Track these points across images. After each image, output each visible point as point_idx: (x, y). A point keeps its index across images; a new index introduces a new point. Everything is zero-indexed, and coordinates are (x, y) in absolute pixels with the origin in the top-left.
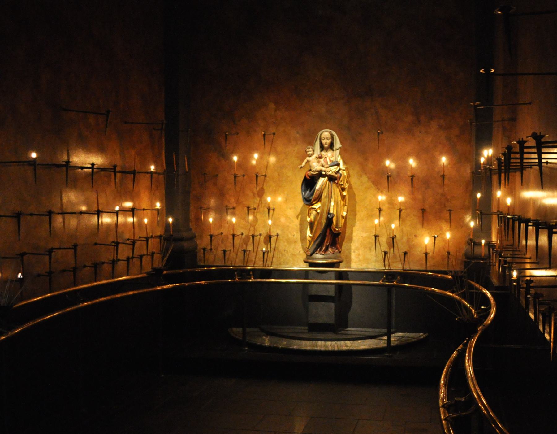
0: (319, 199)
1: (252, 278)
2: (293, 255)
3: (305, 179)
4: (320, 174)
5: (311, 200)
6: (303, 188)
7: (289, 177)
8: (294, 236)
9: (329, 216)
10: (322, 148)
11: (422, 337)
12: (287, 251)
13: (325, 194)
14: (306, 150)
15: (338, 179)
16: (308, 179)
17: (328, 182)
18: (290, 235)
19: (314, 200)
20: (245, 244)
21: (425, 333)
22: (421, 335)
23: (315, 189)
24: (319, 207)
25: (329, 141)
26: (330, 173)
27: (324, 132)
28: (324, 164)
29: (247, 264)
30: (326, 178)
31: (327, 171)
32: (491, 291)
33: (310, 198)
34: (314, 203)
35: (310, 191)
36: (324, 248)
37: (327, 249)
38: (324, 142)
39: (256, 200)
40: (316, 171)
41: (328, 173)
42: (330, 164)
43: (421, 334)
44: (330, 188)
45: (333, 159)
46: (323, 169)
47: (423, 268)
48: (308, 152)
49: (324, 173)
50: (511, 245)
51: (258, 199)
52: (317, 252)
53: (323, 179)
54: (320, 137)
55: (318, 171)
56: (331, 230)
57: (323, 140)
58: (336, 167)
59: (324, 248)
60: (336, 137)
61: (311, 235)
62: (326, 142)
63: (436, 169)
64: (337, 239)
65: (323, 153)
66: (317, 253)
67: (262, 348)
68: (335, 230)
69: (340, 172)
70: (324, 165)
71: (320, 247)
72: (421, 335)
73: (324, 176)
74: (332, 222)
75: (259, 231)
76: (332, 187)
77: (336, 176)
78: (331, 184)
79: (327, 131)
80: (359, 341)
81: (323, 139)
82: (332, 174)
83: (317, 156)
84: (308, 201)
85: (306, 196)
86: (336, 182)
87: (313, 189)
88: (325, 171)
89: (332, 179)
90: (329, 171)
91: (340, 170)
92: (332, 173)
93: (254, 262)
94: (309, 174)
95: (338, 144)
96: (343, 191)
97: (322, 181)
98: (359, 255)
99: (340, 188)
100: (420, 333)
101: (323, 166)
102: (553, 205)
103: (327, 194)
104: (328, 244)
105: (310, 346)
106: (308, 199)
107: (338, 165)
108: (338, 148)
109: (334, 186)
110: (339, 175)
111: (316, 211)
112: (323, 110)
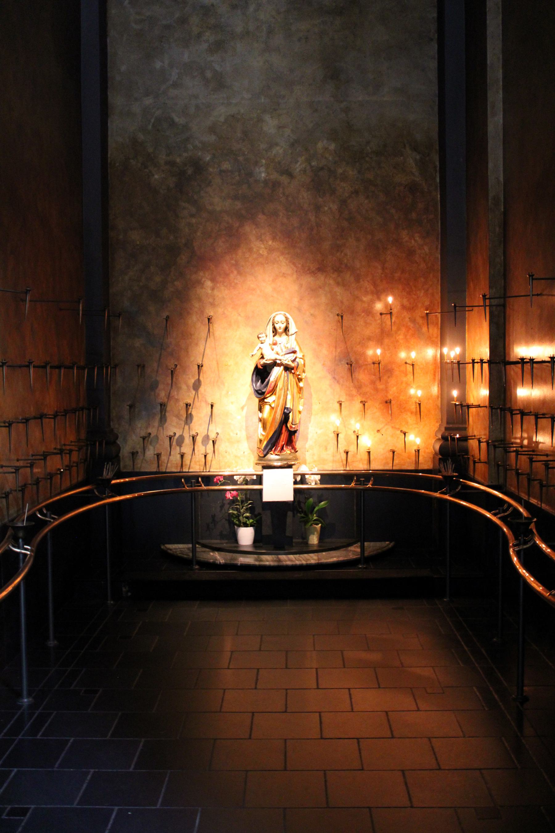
0: (273, 391)
1: (203, 486)
2: (236, 456)
3: (256, 368)
4: (275, 364)
5: (264, 392)
6: (254, 379)
7: (230, 366)
8: (237, 434)
9: (286, 410)
10: (275, 331)
11: (390, 546)
12: (229, 453)
13: (280, 385)
14: (258, 336)
15: (295, 369)
16: (260, 368)
17: (284, 371)
18: (232, 434)
19: (268, 393)
20: (178, 445)
21: (391, 542)
22: (386, 545)
23: (269, 380)
24: (274, 401)
25: (283, 326)
26: (286, 362)
27: (277, 315)
28: (280, 352)
29: (210, 469)
30: (282, 367)
31: (283, 360)
32: (452, 493)
33: (263, 391)
34: (268, 396)
35: (262, 382)
36: (279, 448)
37: (282, 449)
38: (277, 326)
39: (190, 394)
40: (269, 360)
41: (284, 361)
42: (286, 351)
43: (387, 543)
44: (286, 378)
45: (289, 346)
46: (278, 357)
47: (412, 467)
48: (261, 337)
49: (278, 362)
50: (501, 441)
51: (194, 392)
52: (272, 453)
53: (278, 368)
54: (273, 320)
55: (272, 360)
56: (287, 427)
57: (277, 323)
58: (293, 354)
59: (279, 448)
60: (291, 321)
61: (264, 433)
62: (280, 326)
63: (369, 360)
64: (293, 437)
65: (277, 338)
66: (271, 454)
67: (214, 566)
68: (291, 427)
69: (297, 360)
70: (279, 353)
71: (275, 447)
72: (386, 545)
73: (279, 365)
74: (288, 418)
75: (195, 430)
76: (288, 378)
77: (293, 365)
78: (287, 373)
79: (280, 314)
80: (324, 553)
81: (277, 322)
82: (288, 363)
83: (271, 343)
84: (261, 395)
85: (258, 389)
86: (293, 371)
87: (267, 380)
88: (280, 360)
89: (287, 369)
90: (285, 359)
91: (296, 358)
92: (289, 362)
93: (188, 466)
94: (262, 363)
95: (293, 328)
96: (299, 382)
97: (276, 372)
98: (314, 455)
99: (296, 378)
100: (386, 541)
101: (277, 354)
102: (527, 398)
103: (282, 386)
104: (284, 443)
105: (272, 561)
106: (260, 392)
107: (294, 352)
108: (294, 333)
109: (291, 376)
110: (296, 363)
111: (270, 405)
112: (269, 289)
